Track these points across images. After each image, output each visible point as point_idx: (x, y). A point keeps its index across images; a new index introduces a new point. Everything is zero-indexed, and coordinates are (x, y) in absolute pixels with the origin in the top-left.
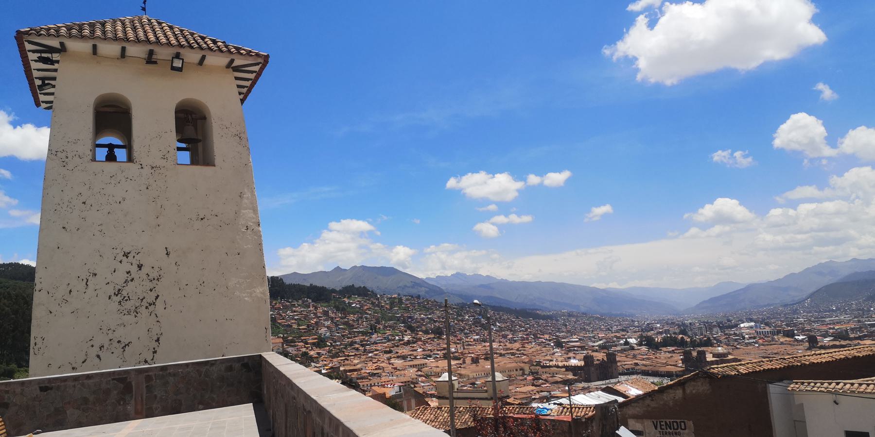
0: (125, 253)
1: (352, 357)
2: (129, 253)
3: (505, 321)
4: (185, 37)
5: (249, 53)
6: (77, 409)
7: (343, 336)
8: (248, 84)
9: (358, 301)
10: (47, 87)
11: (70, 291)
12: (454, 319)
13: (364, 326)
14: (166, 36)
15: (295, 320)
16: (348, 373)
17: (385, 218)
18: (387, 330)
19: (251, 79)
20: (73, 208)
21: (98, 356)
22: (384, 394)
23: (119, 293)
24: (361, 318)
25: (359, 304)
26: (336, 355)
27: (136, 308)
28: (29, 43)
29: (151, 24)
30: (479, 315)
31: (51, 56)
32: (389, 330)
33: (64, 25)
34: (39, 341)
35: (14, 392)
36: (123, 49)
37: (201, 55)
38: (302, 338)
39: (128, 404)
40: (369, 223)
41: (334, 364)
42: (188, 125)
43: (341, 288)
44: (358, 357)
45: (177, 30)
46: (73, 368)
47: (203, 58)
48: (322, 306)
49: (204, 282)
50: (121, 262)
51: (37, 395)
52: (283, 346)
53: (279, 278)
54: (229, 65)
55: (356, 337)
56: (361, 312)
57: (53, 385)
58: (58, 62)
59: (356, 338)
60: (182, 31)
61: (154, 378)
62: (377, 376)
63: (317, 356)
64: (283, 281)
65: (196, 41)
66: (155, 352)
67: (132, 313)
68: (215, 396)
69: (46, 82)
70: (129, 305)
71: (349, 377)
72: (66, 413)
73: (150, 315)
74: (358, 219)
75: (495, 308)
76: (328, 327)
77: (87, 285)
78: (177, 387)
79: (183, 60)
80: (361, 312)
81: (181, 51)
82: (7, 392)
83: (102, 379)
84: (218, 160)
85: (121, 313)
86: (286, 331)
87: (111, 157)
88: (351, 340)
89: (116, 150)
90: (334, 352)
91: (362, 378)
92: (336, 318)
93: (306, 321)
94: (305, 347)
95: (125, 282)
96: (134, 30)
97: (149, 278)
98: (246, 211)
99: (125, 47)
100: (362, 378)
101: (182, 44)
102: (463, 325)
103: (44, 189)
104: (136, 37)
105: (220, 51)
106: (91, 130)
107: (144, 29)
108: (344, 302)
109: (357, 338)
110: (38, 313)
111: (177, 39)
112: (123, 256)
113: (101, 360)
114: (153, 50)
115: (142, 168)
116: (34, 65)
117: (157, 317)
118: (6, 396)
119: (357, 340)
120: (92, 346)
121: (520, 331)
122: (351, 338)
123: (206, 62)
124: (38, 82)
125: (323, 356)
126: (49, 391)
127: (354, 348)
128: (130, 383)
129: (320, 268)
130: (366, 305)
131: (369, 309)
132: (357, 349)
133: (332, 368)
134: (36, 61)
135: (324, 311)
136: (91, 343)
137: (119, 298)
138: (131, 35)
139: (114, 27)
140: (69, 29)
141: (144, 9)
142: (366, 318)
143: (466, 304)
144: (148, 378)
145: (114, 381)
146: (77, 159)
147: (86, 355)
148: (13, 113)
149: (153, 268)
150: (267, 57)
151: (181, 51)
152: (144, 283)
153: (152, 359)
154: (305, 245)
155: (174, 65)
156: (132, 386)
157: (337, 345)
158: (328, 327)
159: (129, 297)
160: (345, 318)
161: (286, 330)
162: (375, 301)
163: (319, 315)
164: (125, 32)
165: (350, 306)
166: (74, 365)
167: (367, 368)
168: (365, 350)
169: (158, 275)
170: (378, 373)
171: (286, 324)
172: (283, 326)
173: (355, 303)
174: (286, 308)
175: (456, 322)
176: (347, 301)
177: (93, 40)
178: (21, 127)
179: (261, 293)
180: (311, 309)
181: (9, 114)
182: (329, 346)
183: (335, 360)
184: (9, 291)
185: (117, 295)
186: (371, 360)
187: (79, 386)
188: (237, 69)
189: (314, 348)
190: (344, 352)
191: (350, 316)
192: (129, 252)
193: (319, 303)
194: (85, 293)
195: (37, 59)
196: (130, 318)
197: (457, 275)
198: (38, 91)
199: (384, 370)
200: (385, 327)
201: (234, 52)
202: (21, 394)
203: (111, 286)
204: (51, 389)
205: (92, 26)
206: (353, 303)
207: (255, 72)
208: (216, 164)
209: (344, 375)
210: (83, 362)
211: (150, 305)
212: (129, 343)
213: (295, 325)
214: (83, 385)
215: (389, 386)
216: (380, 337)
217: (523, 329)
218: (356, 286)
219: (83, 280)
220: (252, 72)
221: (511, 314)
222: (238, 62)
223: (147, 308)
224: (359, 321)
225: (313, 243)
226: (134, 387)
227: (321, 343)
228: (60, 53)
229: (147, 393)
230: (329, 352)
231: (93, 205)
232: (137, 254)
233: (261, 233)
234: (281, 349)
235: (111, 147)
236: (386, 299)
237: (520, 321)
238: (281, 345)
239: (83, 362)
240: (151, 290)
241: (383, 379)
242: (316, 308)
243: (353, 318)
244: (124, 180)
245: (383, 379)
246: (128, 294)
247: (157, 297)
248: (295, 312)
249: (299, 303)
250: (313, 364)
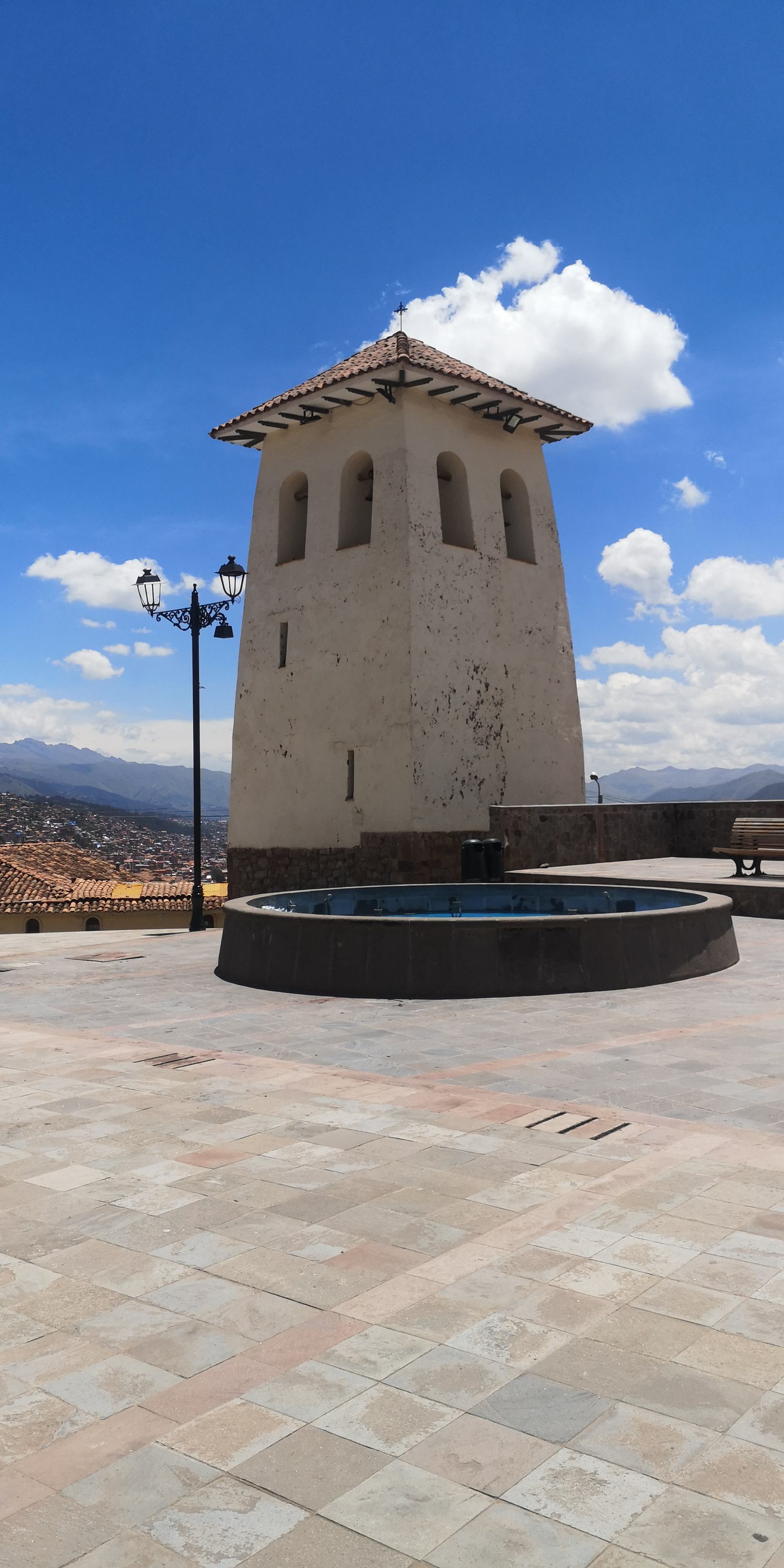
3: (118, 834)
12: (25, 823)
30: (72, 819)
67: (484, 743)
75: (96, 808)
77: (449, 703)
102: (41, 835)
115: (482, 558)
121: (147, 852)
143: (44, 799)
147: (453, 790)
159: (481, 723)
175: (27, 828)
197: (28, 743)
208: (537, 562)
210: (451, 798)
217: (151, 848)
221: (129, 821)
223: (494, 739)
237: (145, 834)
239: (451, 798)
244: (469, 572)
246: (480, 719)
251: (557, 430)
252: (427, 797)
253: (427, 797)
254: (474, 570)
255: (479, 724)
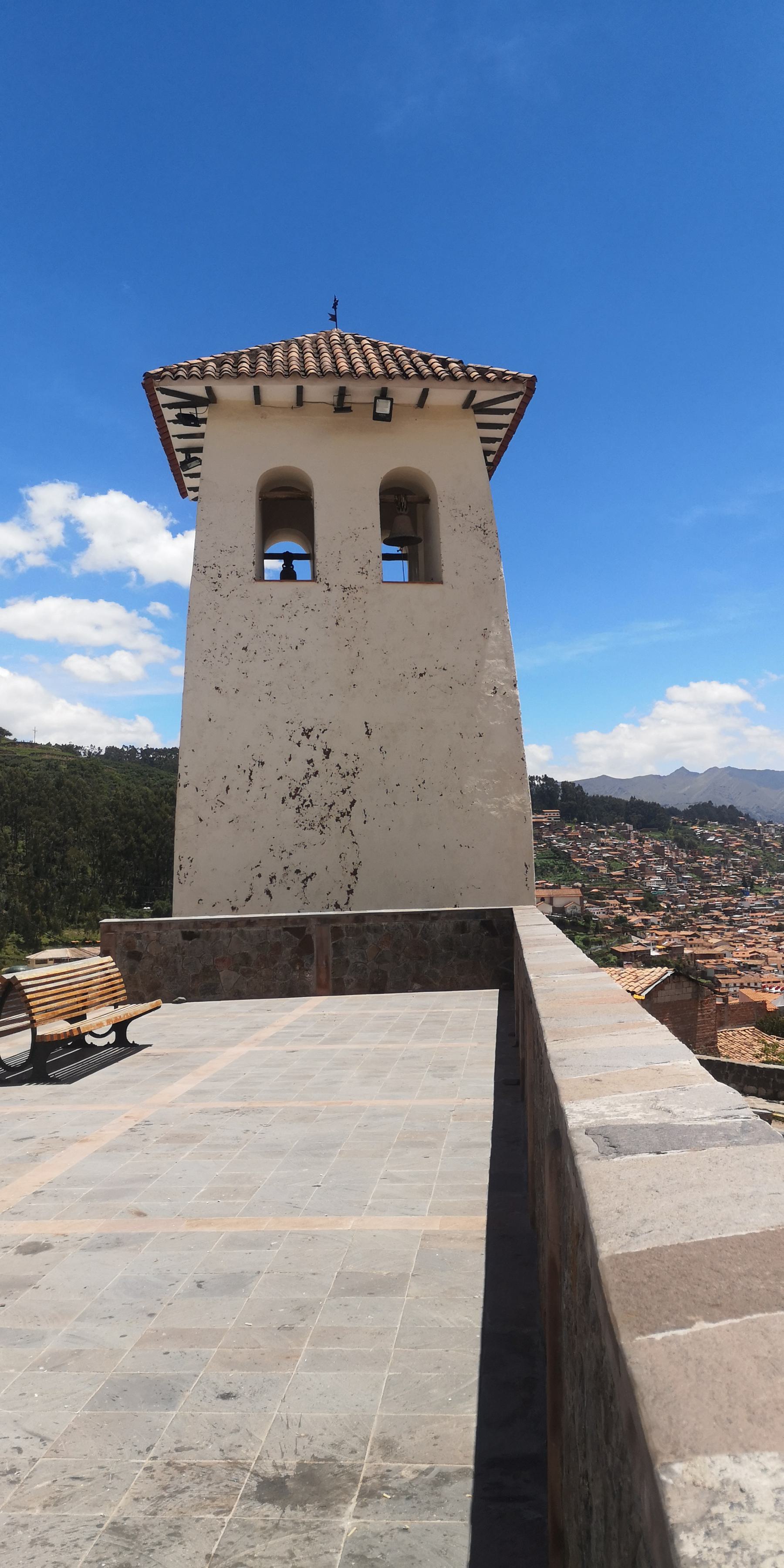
0: (304, 730)
1: (707, 933)
2: (310, 731)
4: (396, 360)
5: (501, 376)
6: (234, 970)
7: (691, 893)
8: (501, 433)
9: (720, 832)
10: (194, 463)
11: (228, 788)
13: (731, 878)
14: (366, 361)
15: (604, 859)
16: (698, 961)
17: (775, 677)
18: (776, 889)
19: (506, 425)
20: (230, 656)
21: (268, 892)
22: (764, 1003)
23: (296, 795)
24: (725, 862)
25: (721, 837)
26: (678, 927)
27: (322, 819)
28: (163, 393)
29: (344, 343)
31: (195, 412)
32: (780, 889)
33: (212, 358)
34: (185, 863)
35: (148, 936)
36: (300, 390)
37: (421, 390)
38: (615, 891)
39: (307, 970)
40: (743, 687)
41: (672, 942)
42: (401, 514)
43: (687, 807)
44: (718, 933)
45: (385, 348)
46: (233, 908)
47: (425, 393)
48: (652, 838)
49: (424, 782)
50: (299, 744)
51: (178, 945)
52: (582, 904)
53: (576, 785)
54: (467, 405)
55: (715, 896)
56: (724, 851)
57: (201, 930)
58: (204, 421)
59: (714, 899)
60: (392, 349)
61: (344, 932)
62: (755, 971)
63: (642, 925)
64: (582, 791)
65: (414, 366)
66: (350, 892)
67: (316, 827)
68: (438, 971)
69: (192, 455)
70: (312, 814)
71: (700, 966)
72: (218, 976)
73: (343, 831)
74: (722, 681)
76: (662, 875)
77: (251, 780)
78: (380, 950)
79: (392, 400)
80: (724, 851)
81: (390, 385)
82: (139, 936)
83: (269, 928)
84: (447, 574)
85: (300, 825)
86: (587, 878)
87: (288, 574)
88: (705, 901)
89: (295, 562)
90: (673, 920)
91: (726, 971)
92: (677, 860)
93: (623, 862)
94: (621, 908)
95: (306, 778)
96: (318, 356)
97: (341, 771)
98: (494, 661)
99: (258, 386)
100: (726, 971)
101: (390, 372)
103: (189, 627)
104: (320, 367)
105: (453, 377)
106: (254, 530)
107: (332, 353)
108: (693, 832)
109: (716, 899)
110: (183, 820)
111: (384, 365)
112: (303, 734)
113: (271, 898)
114: (345, 387)
115: (329, 590)
116: (175, 429)
117: (353, 835)
118: (138, 942)
119: (717, 901)
120: (260, 876)
122: (705, 897)
123: (431, 400)
124: (181, 457)
125: (653, 927)
126: (195, 939)
127: (711, 917)
128: (310, 936)
129: (650, 770)
130: (734, 840)
131: (740, 847)
132: (717, 920)
133: (668, 948)
134: (174, 422)
135: (655, 846)
136: (257, 871)
137: (296, 802)
138: (311, 365)
139: (287, 354)
140: (220, 363)
141: (334, 318)
142: (735, 864)
144: (337, 933)
145: (286, 932)
146: (234, 578)
148: (170, 514)
149: (346, 755)
150: (533, 380)
151: (390, 385)
152: (333, 779)
153: (347, 903)
154: (623, 728)
155: (378, 411)
156: (312, 942)
157: (679, 909)
158: (662, 875)
159: (311, 801)
160: (695, 861)
161: (587, 876)
162: (752, 833)
163: (647, 853)
164: (302, 360)
165: (704, 839)
166: (234, 904)
167: (734, 954)
168: (731, 922)
169: (354, 768)
170: (756, 966)
171: (587, 865)
172: (582, 868)
173: (714, 835)
174: (587, 838)
176: (698, 830)
177: (253, 379)
178: (183, 535)
179: (518, 804)
180: (632, 841)
181: (165, 515)
182: (664, 909)
183: (674, 934)
184: (172, 791)
185: (294, 798)
186: (743, 941)
187: (236, 935)
188: (481, 409)
189: (636, 910)
190: (691, 922)
191: (704, 858)
192: (310, 728)
193: (648, 831)
194: (248, 791)
195: (176, 418)
196: (313, 836)
198: (183, 473)
199: (767, 961)
200: (771, 882)
201: (476, 377)
202: (158, 941)
203: (285, 783)
204: (197, 936)
205: (254, 355)
206: (709, 835)
207: (512, 410)
209: (692, 963)
210: (247, 900)
211: (343, 815)
212: (313, 874)
213: (603, 867)
214: (242, 933)
215: (773, 990)
216: (762, 899)
218: (717, 804)
219: (245, 771)
220: (506, 412)
222: (483, 396)
223: (337, 820)
224: (720, 868)
225: (638, 724)
226: (315, 944)
227: (650, 903)
228: (207, 406)
229: (334, 956)
230: (663, 920)
231: (257, 652)
232: (323, 732)
233: (519, 700)
234: (579, 908)
235: (287, 558)
236: (773, 831)
238: (578, 901)
239: (247, 900)
240: (344, 792)
241: (766, 977)
242: (641, 841)
243: (708, 862)
244: (302, 610)
245: (766, 977)
246: (310, 796)
247: (353, 803)
248: (603, 845)
249: (610, 830)
250: (635, 939)
251: (491, 407)
252: (201, 900)
253: (201, 900)
254: (309, 610)
255: (307, 803)
